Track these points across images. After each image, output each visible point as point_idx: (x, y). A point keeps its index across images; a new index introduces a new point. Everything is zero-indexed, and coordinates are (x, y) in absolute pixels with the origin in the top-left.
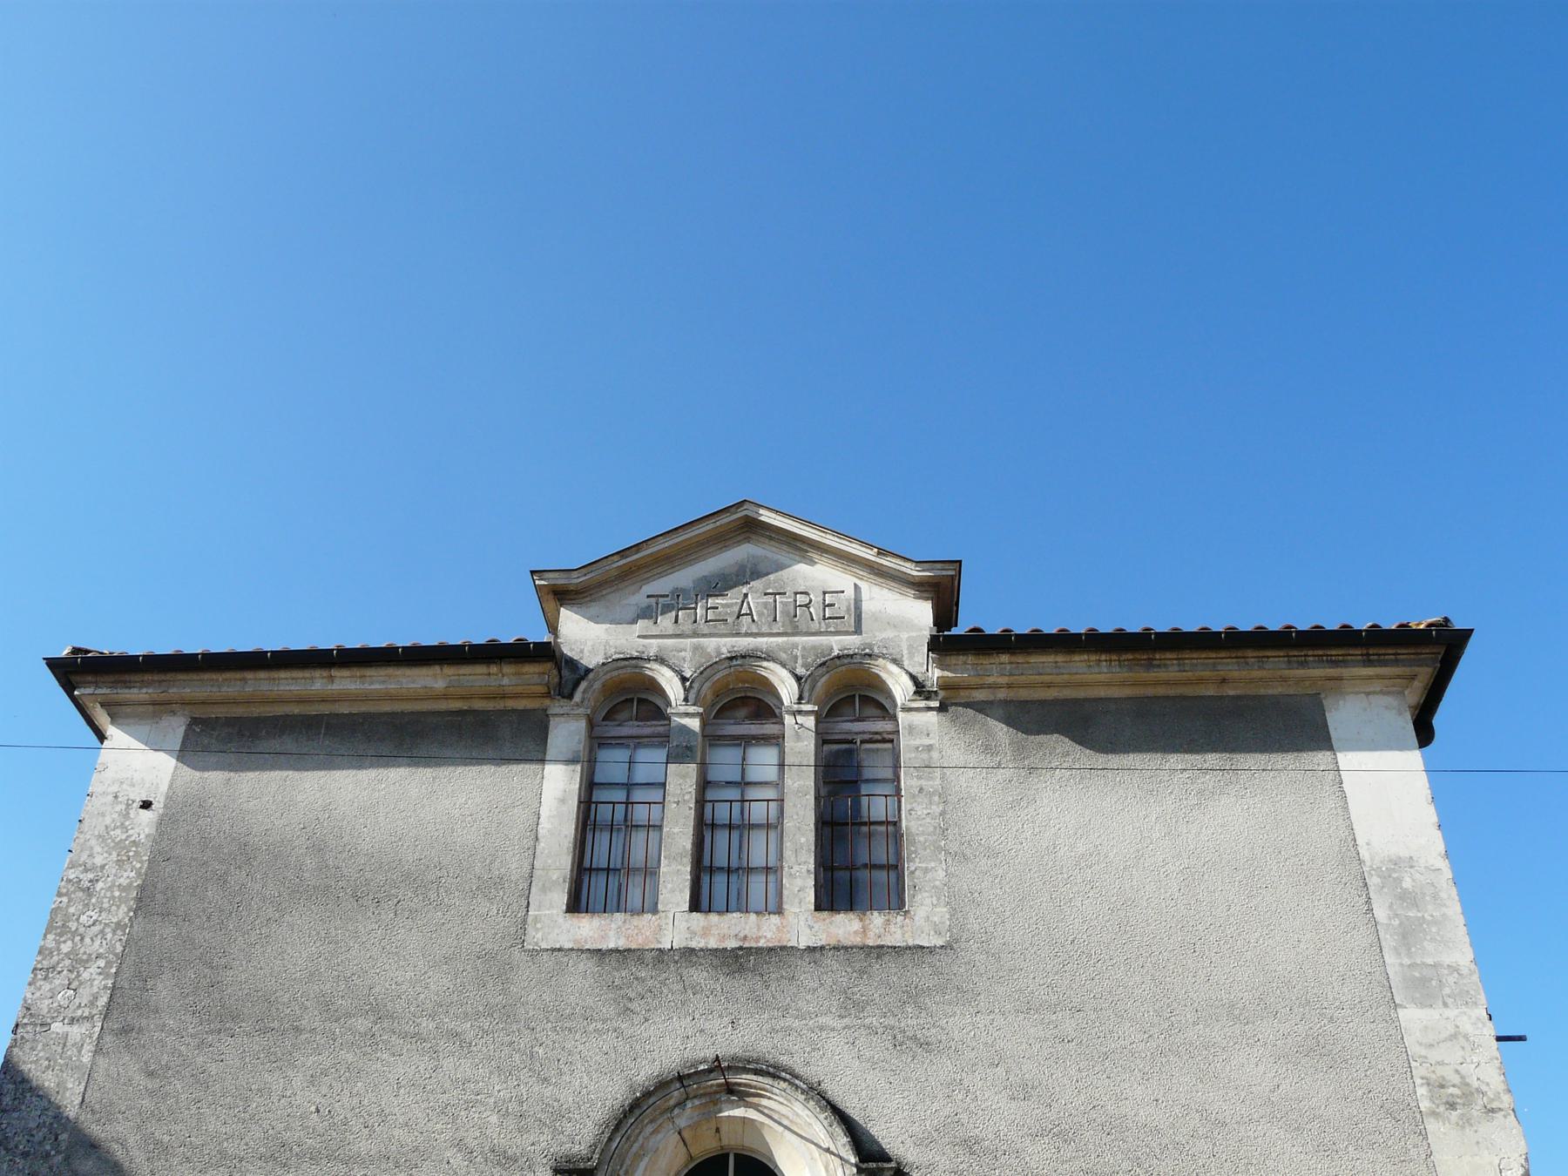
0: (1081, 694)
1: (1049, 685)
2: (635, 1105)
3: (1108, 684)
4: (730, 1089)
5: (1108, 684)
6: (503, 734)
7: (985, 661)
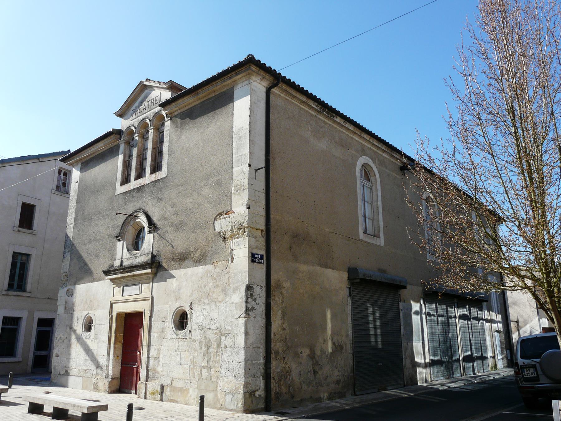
0: (190, 106)
1: (185, 106)
2: (124, 223)
3: (193, 102)
4: (136, 216)
5: (193, 102)
6: (112, 152)
7: (171, 106)
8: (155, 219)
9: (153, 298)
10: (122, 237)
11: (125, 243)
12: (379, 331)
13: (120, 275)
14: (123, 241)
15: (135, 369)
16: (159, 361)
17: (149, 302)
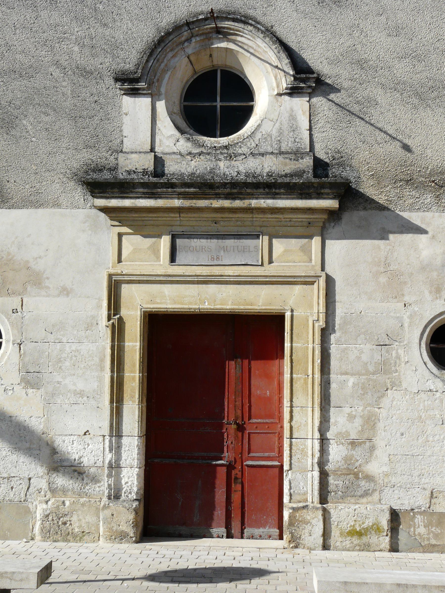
8: (314, 58)
9: (330, 282)
10: (150, 85)
11: (161, 106)
12: (227, 367)
13: (177, 203)
14: (155, 97)
15: (222, 473)
16: (372, 449)
17: (318, 290)
